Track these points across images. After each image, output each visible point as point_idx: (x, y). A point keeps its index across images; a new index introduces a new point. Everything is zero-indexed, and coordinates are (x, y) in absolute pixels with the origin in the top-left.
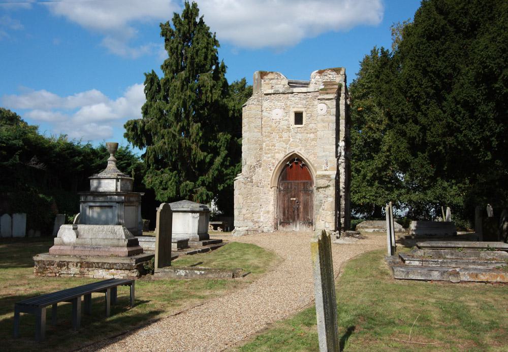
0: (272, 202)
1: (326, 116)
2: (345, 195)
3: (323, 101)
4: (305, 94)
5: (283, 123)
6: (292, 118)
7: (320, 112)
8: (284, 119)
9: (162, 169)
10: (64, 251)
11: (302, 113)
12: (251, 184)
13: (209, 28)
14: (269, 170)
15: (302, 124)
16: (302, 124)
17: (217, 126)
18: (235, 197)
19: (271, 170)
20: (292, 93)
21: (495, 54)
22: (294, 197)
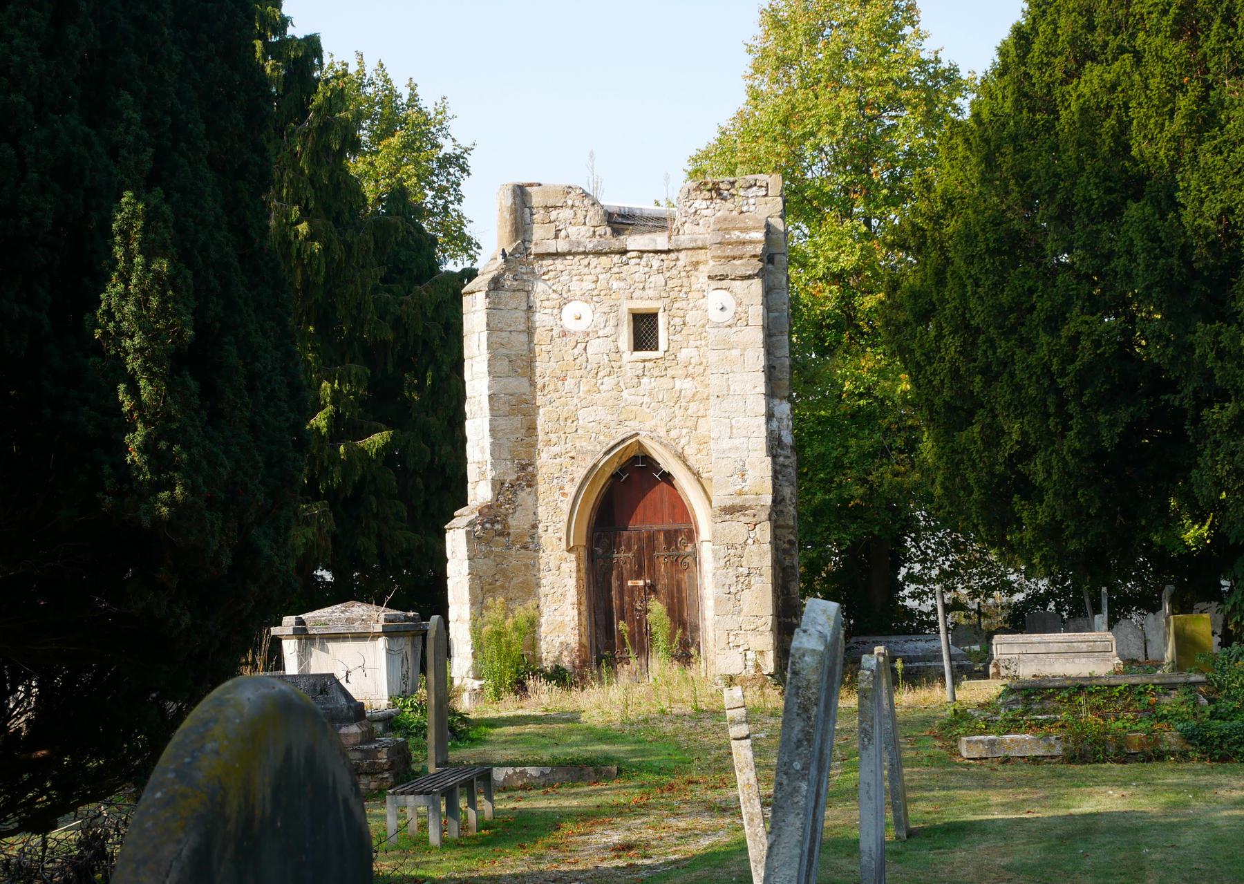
0: (572, 595)
1: (734, 329)
2: (27, 728)
3: (725, 283)
4: (664, 256)
5: (595, 346)
6: (625, 337)
7: (715, 315)
8: (601, 333)
9: (883, 208)
10: (1103, 680)
11: (655, 315)
12: (503, 540)
13: (312, 45)
14: (557, 494)
15: (657, 349)
16: (657, 349)
17: (184, 456)
18: (450, 582)
19: (564, 494)
20: (624, 252)
21: (586, 388)
22: (638, 577)
